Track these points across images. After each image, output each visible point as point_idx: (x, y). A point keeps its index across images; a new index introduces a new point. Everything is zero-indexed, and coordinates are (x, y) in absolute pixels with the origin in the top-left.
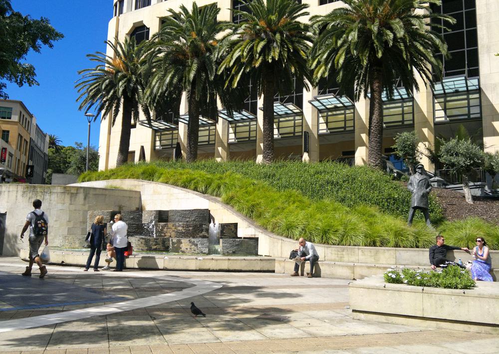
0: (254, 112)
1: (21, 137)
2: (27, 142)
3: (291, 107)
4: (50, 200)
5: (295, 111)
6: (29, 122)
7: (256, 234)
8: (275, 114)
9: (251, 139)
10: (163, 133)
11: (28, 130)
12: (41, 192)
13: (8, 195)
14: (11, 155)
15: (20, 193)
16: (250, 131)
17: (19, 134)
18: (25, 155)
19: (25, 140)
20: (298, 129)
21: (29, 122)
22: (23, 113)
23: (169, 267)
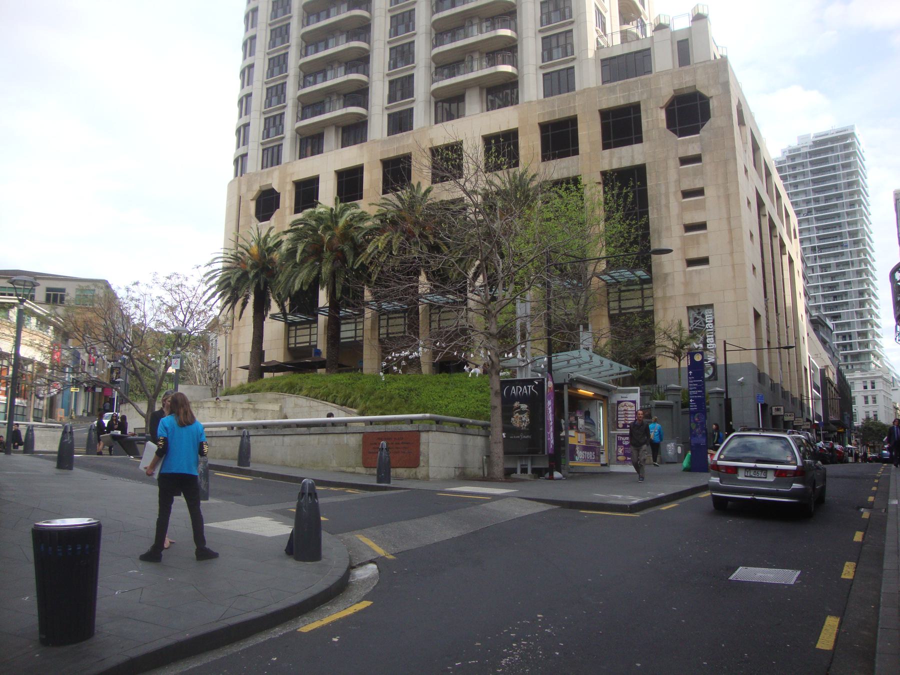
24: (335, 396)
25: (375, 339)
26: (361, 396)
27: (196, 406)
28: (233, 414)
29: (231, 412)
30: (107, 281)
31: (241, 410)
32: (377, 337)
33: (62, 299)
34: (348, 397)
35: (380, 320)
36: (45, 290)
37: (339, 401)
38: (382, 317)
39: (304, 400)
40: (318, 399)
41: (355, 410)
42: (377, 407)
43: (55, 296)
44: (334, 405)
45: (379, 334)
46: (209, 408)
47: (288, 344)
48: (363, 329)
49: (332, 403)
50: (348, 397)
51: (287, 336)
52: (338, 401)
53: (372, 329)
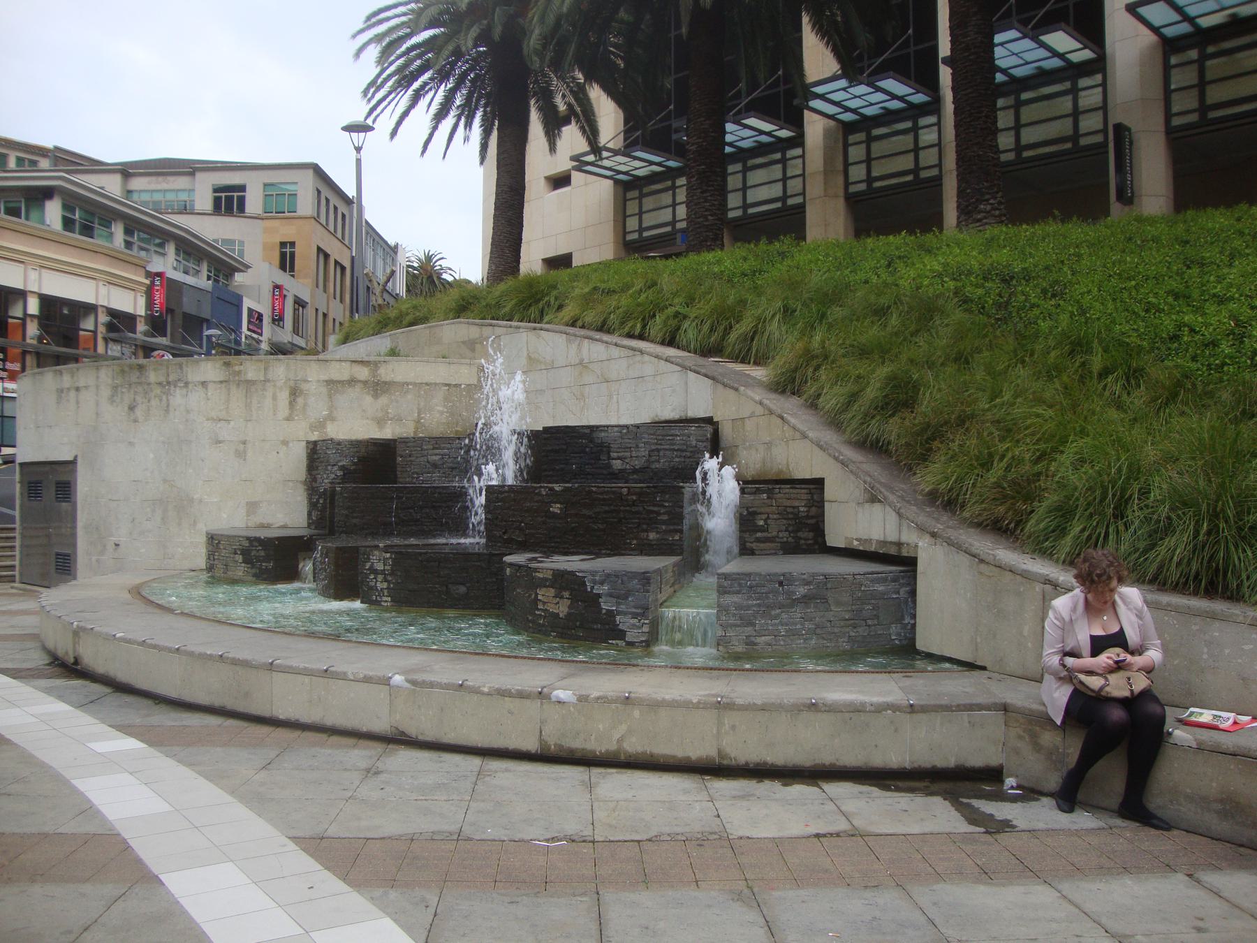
0: (928, 81)
1: (327, 256)
2: (343, 269)
3: (1061, 40)
4: (188, 412)
5: (1076, 58)
6: (344, 216)
7: (904, 539)
8: (999, 77)
9: (924, 174)
10: (646, 190)
11: (335, 231)
12: (160, 384)
13: (78, 402)
14: (300, 303)
15: (106, 392)
16: (916, 150)
17: (319, 249)
18: (342, 301)
19: (336, 262)
20: (1090, 123)
21: (344, 216)
22: (326, 193)
23: (413, 730)
24: (677, 315)
25: (836, 196)
26: (787, 312)
27: (162, 379)
28: (292, 404)
29: (284, 396)
30: (317, 165)
31: (324, 390)
32: (841, 192)
33: (242, 201)
34: (726, 316)
35: (846, 146)
36: (211, 191)
37: (691, 334)
38: (852, 139)
39: (560, 340)
40: (609, 332)
41: (759, 373)
42: (863, 352)
43: (229, 200)
44: (671, 352)
45: (847, 184)
46: (204, 384)
47: (625, 233)
48: (803, 175)
49: (662, 343)
50: (726, 316)
51: (621, 214)
52: (690, 332)
53: (828, 171)
